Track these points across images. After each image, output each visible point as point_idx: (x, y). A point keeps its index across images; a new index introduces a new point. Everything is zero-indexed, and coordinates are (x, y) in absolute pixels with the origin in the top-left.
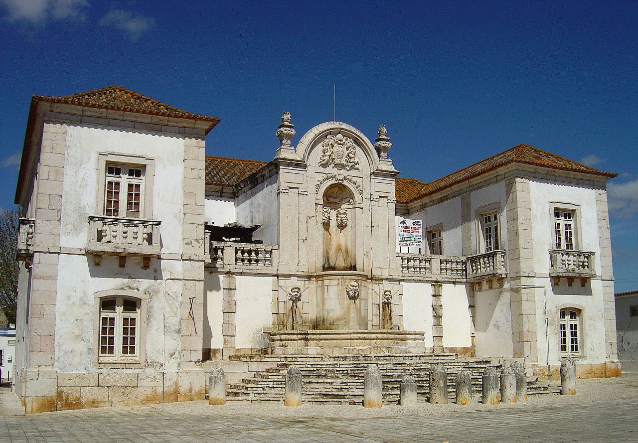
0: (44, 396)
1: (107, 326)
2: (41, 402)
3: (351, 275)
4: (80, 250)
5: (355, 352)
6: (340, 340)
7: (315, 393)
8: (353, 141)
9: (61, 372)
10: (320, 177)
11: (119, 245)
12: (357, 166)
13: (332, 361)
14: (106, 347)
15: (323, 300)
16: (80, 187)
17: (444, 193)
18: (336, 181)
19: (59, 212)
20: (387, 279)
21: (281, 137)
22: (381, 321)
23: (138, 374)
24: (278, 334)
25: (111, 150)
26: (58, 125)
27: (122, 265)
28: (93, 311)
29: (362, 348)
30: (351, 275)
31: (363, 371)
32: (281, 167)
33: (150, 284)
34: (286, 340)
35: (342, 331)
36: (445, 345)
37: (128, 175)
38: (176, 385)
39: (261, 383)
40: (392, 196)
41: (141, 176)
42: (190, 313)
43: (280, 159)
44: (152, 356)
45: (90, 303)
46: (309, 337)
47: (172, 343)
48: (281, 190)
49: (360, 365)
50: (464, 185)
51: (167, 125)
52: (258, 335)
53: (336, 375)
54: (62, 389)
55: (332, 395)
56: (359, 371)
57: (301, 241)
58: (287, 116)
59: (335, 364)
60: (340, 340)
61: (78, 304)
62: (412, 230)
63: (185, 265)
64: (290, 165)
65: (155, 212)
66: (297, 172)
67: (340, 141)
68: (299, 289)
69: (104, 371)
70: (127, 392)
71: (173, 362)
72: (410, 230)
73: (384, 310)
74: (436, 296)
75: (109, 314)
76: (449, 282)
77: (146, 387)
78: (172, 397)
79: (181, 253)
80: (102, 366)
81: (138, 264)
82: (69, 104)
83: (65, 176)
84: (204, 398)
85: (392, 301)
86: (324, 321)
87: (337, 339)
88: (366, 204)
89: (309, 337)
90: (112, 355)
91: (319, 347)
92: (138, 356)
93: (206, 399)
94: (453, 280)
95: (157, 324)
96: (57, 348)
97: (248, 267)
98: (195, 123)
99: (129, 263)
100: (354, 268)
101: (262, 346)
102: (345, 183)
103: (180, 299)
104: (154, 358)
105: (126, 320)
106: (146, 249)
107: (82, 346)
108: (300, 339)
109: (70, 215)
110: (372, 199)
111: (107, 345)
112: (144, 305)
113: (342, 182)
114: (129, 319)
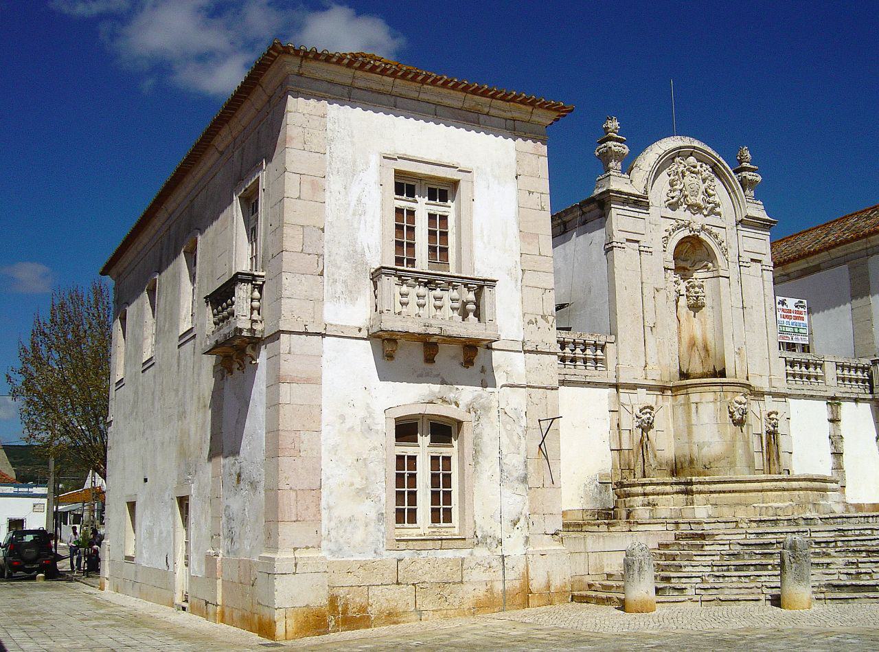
0: (307, 606)
1: (405, 468)
2: (301, 618)
3: (715, 384)
4: (360, 330)
5: (771, 512)
6: (745, 492)
7: (817, 584)
8: (710, 169)
9: (334, 559)
10: (668, 225)
11: (433, 322)
12: (718, 210)
13: (754, 528)
14: (405, 514)
15: (689, 427)
16: (354, 214)
17: (813, 261)
18: (690, 232)
19: (321, 259)
20: (769, 394)
21: (606, 158)
22: (765, 461)
23: (463, 560)
24: (639, 485)
25: (401, 151)
26: (312, 102)
27: (430, 359)
28: (383, 443)
29: (780, 505)
30: (715, 384)
31: (865, 543)
32: (612, 206)
33: (476, 393)
34: (653, 494)
35: (726, 477)
36: (849, 501)
37: (427, 198)
38: (526, 578)
39: (687, 569)
40: (767, 260)
41: (449, 201)
42: (540, 446)
43: (613, 191)
44: (486, 525)
45: (379, 427)
46: (694, 488)
47: (514, 501)
48: (614, 244)
49: (850, 532)
50: (857, 246)
51: (487, 114)
52: (592, 487)
53: (824, 550)
54: (335, 591)
55: (852, 585)
56: (858, 543)
57: (648, 330)
58: (613, 124)
59: (803, 532)
60: (745, 492)
61: (359, 430)
62: (794, 315)
63: (528, 361)
64: (625, 202)
65: (478, 265)
66: (636, 215)
67: (695, 167)
68: (652, 408)
69: (406, 555)
70: (445, 593)
71: (518, 535)
72: (792, 314)
73: (768, 444)
74: (834, 421)
75: (408, 450)
76: (849, 399)
77: (476, 583)
78: (519, 600)
79: (521, 339)
80: (402, 545)
81: (454, 357)
82: (334, 63)
83: (328, 194)
84: (570, 600)
85: (779, 430)
86: (691, 462)
87: (740, 491)
88: (733, 271)
89: (694, 488)
90: (414, 525)
91: (710, 506)
92: (457, 525)
93: (572, 601)
94: (855, 396)
95: (489, 466)
96: (324, 514)
97: (573, 371)
98: (532, 113)
99: (445, 356)
100: (722, 374)
101: (598, 505)
102: (702, 236)
103: (524, 423)
104: (486, 528)
105: (434, 459)
106: (471, 329)
107: (368, 509)
108: (677, 493)
109: (339, 265)
110: (741, 263)
111: (406, 506)
112: (467, 431)
113: (698, 234)
114: (441, 458)
